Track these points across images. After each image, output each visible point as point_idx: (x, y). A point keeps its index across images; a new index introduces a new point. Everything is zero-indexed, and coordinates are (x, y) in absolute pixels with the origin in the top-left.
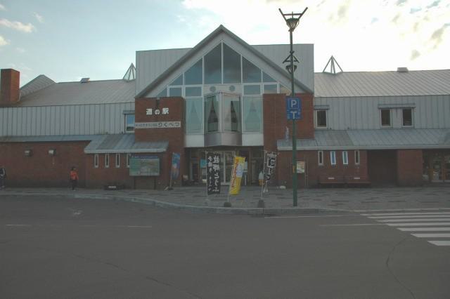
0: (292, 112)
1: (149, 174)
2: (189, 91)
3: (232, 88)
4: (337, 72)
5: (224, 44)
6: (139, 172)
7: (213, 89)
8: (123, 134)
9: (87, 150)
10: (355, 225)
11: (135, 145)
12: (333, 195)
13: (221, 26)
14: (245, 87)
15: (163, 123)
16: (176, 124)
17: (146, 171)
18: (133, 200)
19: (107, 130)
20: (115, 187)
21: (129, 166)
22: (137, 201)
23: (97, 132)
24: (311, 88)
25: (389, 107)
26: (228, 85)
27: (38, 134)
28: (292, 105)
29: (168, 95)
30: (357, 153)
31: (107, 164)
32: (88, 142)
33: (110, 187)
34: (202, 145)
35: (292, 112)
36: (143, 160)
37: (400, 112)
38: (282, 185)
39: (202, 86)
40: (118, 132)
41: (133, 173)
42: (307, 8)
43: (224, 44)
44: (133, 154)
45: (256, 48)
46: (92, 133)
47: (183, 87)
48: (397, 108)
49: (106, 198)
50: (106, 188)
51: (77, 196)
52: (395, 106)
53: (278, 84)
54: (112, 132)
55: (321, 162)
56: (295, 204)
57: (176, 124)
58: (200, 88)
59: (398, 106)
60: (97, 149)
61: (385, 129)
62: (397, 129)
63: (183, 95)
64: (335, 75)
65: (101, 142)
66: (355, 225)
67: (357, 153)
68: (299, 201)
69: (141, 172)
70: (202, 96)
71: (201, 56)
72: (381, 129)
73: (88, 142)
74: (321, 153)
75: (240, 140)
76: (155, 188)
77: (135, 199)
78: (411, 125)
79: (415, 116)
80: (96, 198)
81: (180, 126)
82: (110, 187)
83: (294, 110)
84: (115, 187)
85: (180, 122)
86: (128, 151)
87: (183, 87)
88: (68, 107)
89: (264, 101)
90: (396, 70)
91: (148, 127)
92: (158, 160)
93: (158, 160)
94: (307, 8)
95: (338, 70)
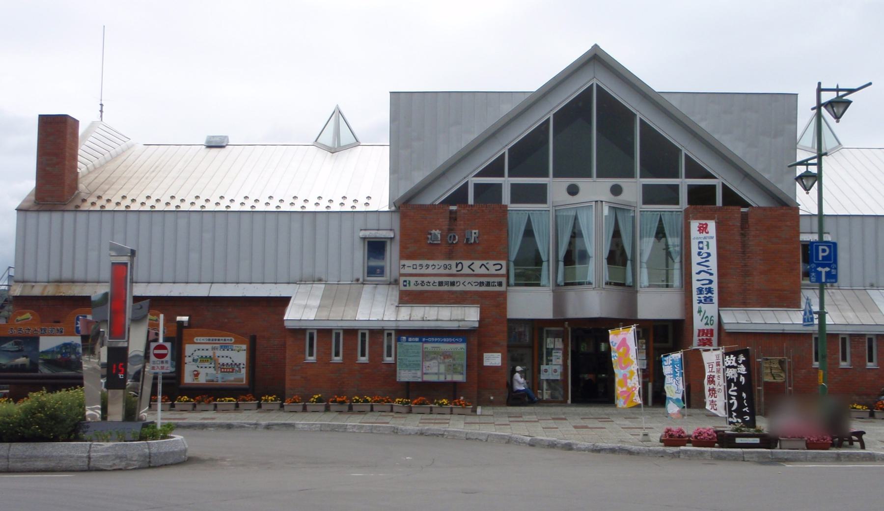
0: (819, 269)
1: (442, 379)
3: (616, 190)
5: (598, 86)
6: (419, 373)
10: (361, 475)
13: (596, 47)
14: (645, 187)
15: (466, 263)
17: (435, 370)
20: (757, 440)
21: (389, 360)
24: (791, 196)
26: (608, 183)
28: (821, 254)
34: (548, 314)
35: (819, 269)
36: (429, 346)
42: (870, 84)
43: (598, 86)
44: (403, 333)
45: (666, 97)
58: (544, 187)
66: (361, 475)
69: (423, 374)
71: (546, 113)
75: (632, 304)
83: (823, 266)
84: (757, 440)
92: (462, 347)
93: (462, 347)
94: (870, 84)
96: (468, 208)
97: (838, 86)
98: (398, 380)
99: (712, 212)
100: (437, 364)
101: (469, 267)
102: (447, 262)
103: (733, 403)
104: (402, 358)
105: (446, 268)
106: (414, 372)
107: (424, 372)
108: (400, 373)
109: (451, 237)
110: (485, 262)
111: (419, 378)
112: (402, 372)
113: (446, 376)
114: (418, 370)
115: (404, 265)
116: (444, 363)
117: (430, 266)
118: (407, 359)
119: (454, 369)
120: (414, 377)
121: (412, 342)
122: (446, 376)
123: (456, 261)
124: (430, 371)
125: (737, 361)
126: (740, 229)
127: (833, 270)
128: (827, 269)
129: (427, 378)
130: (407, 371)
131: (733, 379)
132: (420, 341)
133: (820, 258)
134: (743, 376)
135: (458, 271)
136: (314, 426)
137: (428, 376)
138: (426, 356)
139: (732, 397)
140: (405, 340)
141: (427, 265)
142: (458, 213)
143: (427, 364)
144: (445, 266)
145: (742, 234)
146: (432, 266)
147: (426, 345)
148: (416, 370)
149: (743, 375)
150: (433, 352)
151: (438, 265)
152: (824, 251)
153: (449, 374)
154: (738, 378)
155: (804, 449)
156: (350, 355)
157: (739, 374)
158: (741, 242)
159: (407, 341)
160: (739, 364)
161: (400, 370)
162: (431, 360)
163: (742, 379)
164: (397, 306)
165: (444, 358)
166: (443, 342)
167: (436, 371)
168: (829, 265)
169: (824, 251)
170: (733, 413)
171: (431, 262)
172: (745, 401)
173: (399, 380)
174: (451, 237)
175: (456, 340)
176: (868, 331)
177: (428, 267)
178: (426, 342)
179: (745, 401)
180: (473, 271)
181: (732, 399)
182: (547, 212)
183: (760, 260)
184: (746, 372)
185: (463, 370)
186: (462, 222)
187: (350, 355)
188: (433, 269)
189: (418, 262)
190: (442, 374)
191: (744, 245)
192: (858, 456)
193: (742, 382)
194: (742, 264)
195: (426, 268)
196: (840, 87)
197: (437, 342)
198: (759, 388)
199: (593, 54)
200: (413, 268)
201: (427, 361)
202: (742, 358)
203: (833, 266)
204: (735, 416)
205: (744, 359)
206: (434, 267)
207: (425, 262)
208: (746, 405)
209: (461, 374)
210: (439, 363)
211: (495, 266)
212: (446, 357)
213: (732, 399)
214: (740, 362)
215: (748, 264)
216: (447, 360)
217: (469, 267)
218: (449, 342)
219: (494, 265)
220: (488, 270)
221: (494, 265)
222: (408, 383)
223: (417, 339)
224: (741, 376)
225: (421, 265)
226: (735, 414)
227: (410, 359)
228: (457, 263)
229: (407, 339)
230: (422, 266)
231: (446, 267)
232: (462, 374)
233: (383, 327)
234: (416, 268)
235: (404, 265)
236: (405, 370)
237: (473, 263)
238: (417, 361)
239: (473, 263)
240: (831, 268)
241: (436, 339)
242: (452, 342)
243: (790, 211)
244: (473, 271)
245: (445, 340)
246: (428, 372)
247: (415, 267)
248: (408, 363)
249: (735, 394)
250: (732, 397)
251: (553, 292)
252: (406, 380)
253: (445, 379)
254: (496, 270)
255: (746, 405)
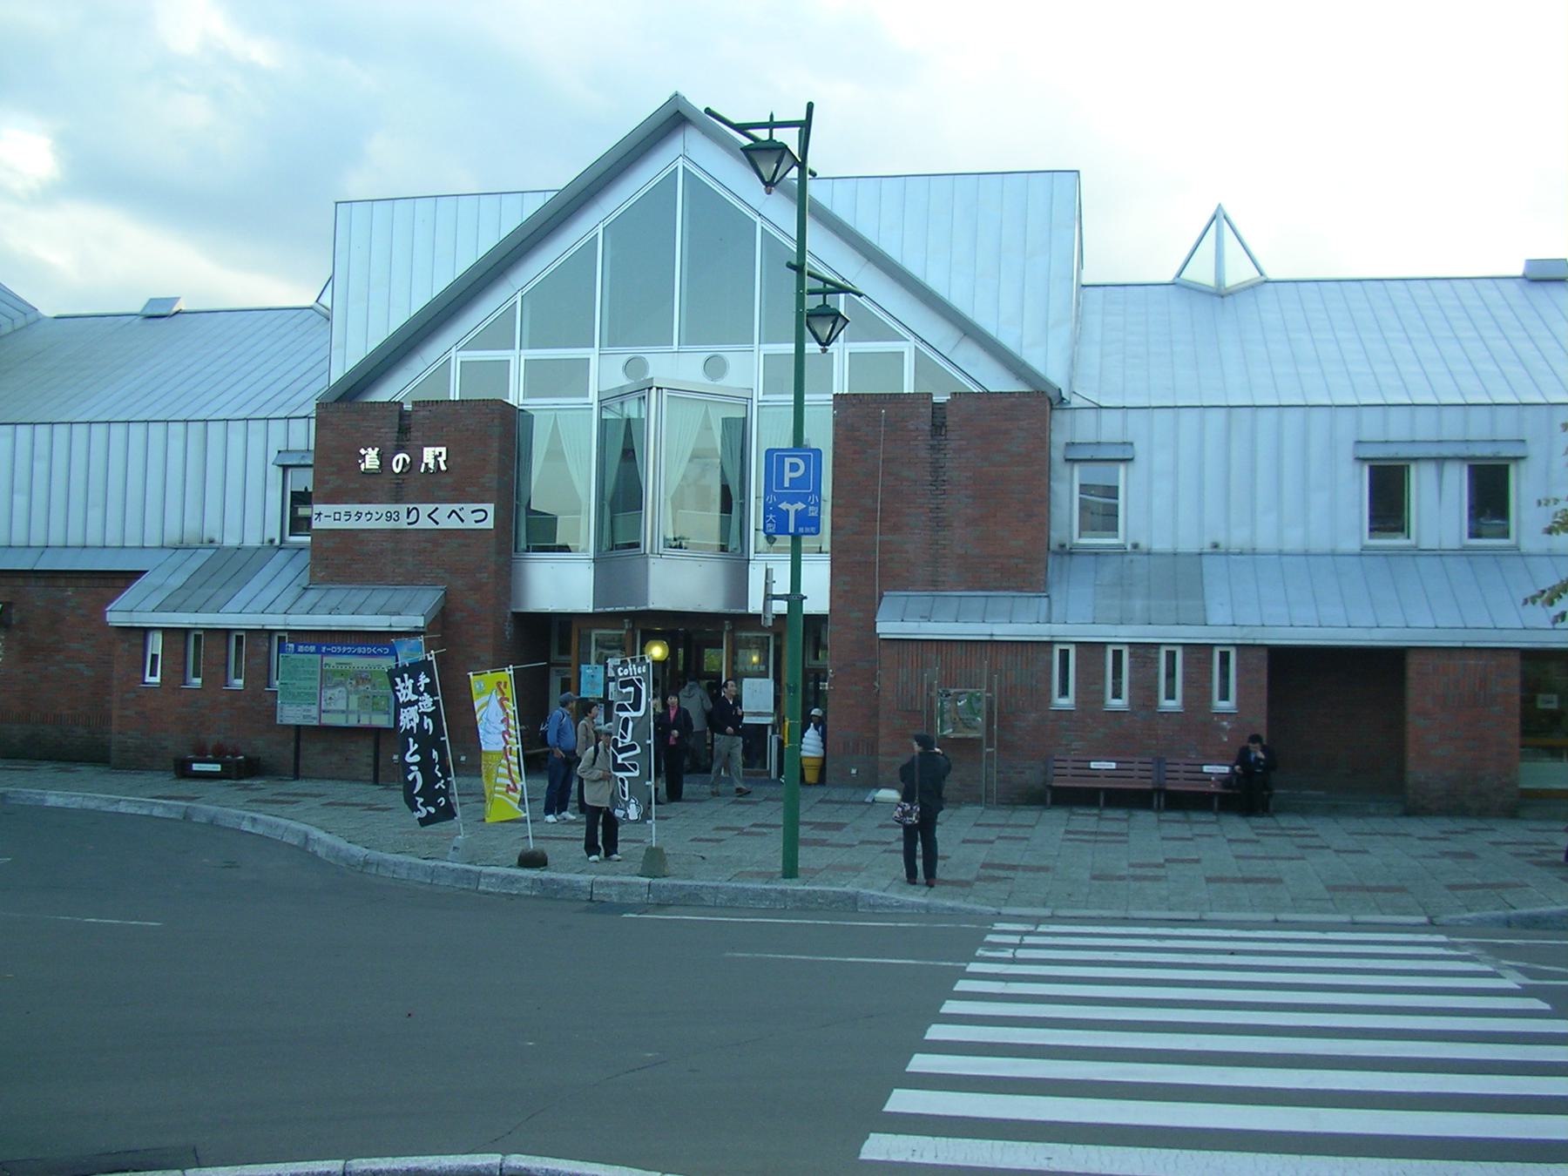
0: (784, 506)
1: (353, 722)
2: (541, 377)
3: (715, 367)
4: (1231, 280)
6: (314, 711)
7: (634, 366)
8: (272, 547)
9: (116, 616)
11: (311, 597)
12: (329, 783)
15: (425, 509)
16: (477, 516)
17: (342, 705)
18: (246, 826)
19: (212, 530)
20: (217, 768)
22: (259, 830)
23: (173, 536)
25: (1507, 451)
27: (75, 539)
28: (788, 475)
29: (455, 395)
30: (1225, 658)
31: (237, 676)
32: (130, 577)
33: (196, 767)
37: (1457, 481)
38: (889, 786)
39: (592, 354)
40: (253, 540)
41: (291, 714)
44: (299, 636)
46: (153, 539)
47: (517, 359)
48: (1440, 460)
49: (158, 812)
50: (183, 770)
51: (54, 799)
52: (1434, 451)
53: (908, 348)
54: (231, 540)
55: (1064, 692)
56: (790, 871)
57: (477, 516)
59: (1446, 451)
60: (160, 608)
61: (1386, 554)
62: (1439, 554)
63: (516, 396)
64: (1220, 294)
65: (177, 581)
67: (1225, 658)
68: (806, 857)
69: (321, 711)
70: (593, 398)
72: (1365, 552)
73: (130, 577)
74: (1064, 655)
76: (376, 781)
77: (254, 820)
78: (1506, 535)
79: (1523, 489)
80: (122, 808)
81: (489, 524)
82: (196, 767)
84: (217, 768)
85: (490, 508)
86: (275, 621)
87: (517, 359)
88: (61, 431)
89: (837, 424)
90: (1519, 270)
91: (363, 524)
95: (1238, 272)
96: (430, 408)
97: (772, 116)
98: (278, 722)
99: (875, 405)
100: (345, 695)
101: (429, 516)
102: (392, 508)
103: (415, 778)
104: (286, 681)
105: (389, 519)
106: (305, 707)
107: (323, 708)
108: (282, 709)
109: (398, 461)
110: (456, 507)
111: (314, 718)
112: (286, 707)
113: (359, 717)
114: (314, 704)
115: (320, 514)
116: (357, 692)
117: (364, 514)
118: (294, 684)
119: (373, 703)
120: (304, 717)
121: (304, 653)
122: (359, 717)
123: (408, 506)
124: (332, 707)
125: (416, 690)
126: (929, 438)
127: (811, 508)
128: (800, 506)
129: (328, 720)
130: (294, 706)
131: (412, 728)
132: (318, 651)
133: (787, 484)
134: (428, 717)
135: (409, 524)
136: (74, 799)
137: (329, 715)
138: (326, 678)
139: (412, 768)
140: (293, 650)
141: (358, 513)
142: (413, 416)
143: (328, 693)
144: (389, 515)
145: (932, 447)
146: (366, 514)
147: (327, 659)
148: (309, 704)
149: (429, 715)
150: (338, 671)
151: (377, 513)
152: (794, 467)
153: (364, 713)
154: (421, 724)
155: (770, 877)
156: (216, 678)
157: (421, 715)
158: (932, 463)
159: (296, 651)
160: (421, 694)
161: (282, 703)
162: (334, 687)
163: (428, 723)
164: (304, 588)
165: (357, 683)
166: (356, 653)
167: (344, 708)
168: (803, 498)
169: (794, 467)
170: (417, 798)
171: (364, 508)
172: (437, 767)
173: (281, 721)
174: (398, 461)
175: (379, 650)
176: (1222, 638)
177: (360, 518)
178: (328, 653)
179: (437, 767)
180: (437, 523)
181: (412, 771)
182: (586, 412)
183: (967, 497)
184: (434, 708)
185: (388, 707)
186: (419, 434)
187: (1145, 694)
188: (347, 520)
189: (343, 508)
190: (352, 712)
191: (936, 468)
192: (822, 898)
193: (428, 730)
194: (931, 506)
195: (357, 518)
196: (776, 119)
197: (346, 653)
198: (988, 750)
199: (672, 110)
200: (335, 520)
201: (331, 688)
202: (424, 680)
203: (812, 499)
204: (422, 804)
205: (428, 680)
206: (369, 516)
207: (354, 508)
208: (440, 775)
209: (385, 714)
210: (349, 693)
211: (475, 514)
212: (361, 681)
213: (412, 771)
214: (422, 689)
215: (944, 506)
216: (361, 688)
217: (429, 516)
218: (366, 655)
219: (473, 512)
220: (462, 521)
221: (473, 512)
222: (298, 729)
223: (313, 648)
224: (425, 717)
225: (348, 514)
226: (420, 800)
227: (303, 683)
228: (408, 509)
229: (296, 648)
230: (350, 515)
231: (391, 516)
232: (388, 713)
233: (263, 625)
234: (340, 520)
235: (320, 514)
236: (290, 704)
237: (437, 509)
238: (311, 688)
239: (437, 509)
240: (809, 504)
241: (345, 649)
242: (372, 655)
243: (1028, 399)
244: (437, 523)
245: (359, 650)
246: (330, 708)
247: (337, 516)
248: (296, 691)
249: (417, 758)
250: (412, 768)
251: (594, 562)
252: (293, 722)
253: (359, 721)
254: (476, 522)
255: (440, 775)
